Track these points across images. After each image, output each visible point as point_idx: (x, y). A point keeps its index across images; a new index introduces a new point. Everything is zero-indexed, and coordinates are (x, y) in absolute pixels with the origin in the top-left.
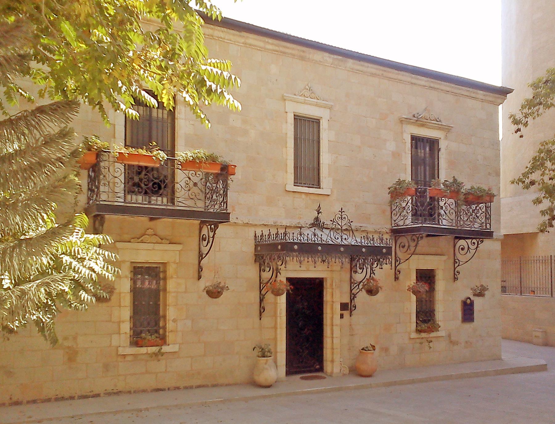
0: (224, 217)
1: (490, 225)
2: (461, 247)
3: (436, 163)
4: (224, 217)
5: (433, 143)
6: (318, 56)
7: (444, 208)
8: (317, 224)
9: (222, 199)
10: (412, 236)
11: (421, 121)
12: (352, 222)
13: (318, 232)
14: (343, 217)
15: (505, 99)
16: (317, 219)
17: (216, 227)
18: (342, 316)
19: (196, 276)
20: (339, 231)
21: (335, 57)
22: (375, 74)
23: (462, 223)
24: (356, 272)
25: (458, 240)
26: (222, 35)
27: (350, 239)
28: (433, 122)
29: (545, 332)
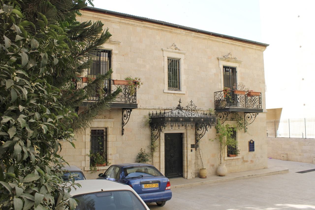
0: (135, 106)
1: (261, 106)
2: (248, 117)
3: (235, 78)
4: (135, 106)
5: (234, 70)
6: (179, 31)
7: (240, 99)
8: (179, 108)
9: (133, 98)
10: (225, 113)
11: (228, 59)
12: (196, 107)
13: (180, 112)
14: (192, 104)
15: (266, 49)
16: (179, 105)
17: (131, 110)
18: (192, 151)
19: (121, 133)
20: (190, 111)
21: (187, 31)
22: (205, 38)
23: (248, 105)
24: (198, 130)
25: (106, 73)
26: (133, 23)
27: (196, 115)
28: (233, 59)
29: (287, 154)
